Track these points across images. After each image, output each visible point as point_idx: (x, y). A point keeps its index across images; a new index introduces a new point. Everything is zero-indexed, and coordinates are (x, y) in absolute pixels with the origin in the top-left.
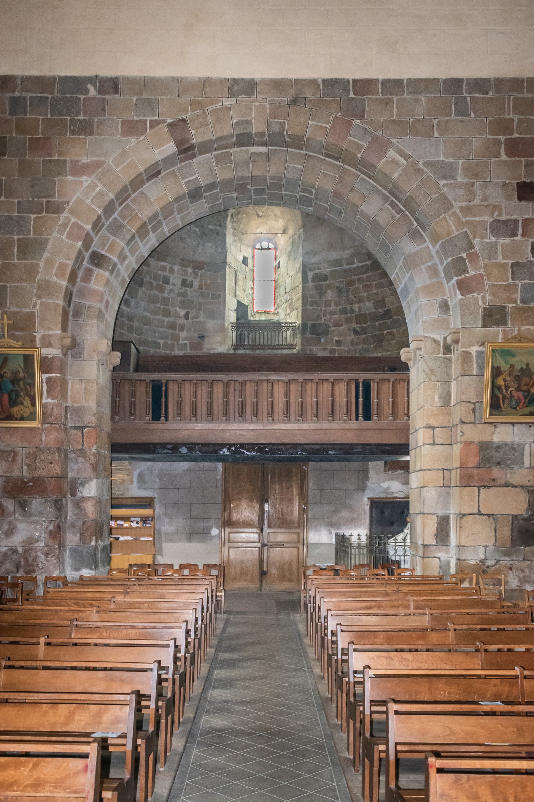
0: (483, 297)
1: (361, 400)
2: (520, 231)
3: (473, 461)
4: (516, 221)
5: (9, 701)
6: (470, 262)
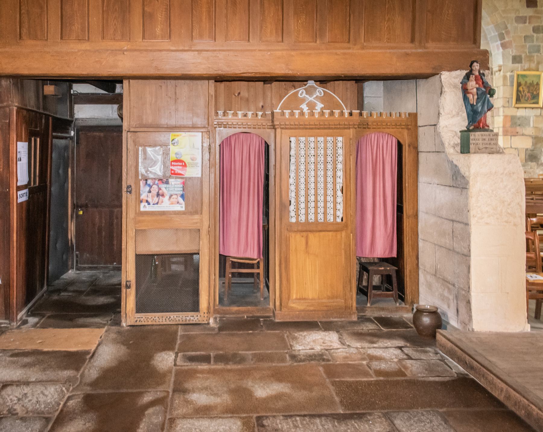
0: (512, 51)
1: (47, 222)
2: (528, 21)
3: (508, 124)
4: (526, 17)
5: (381, 246)
6: (506, 34)
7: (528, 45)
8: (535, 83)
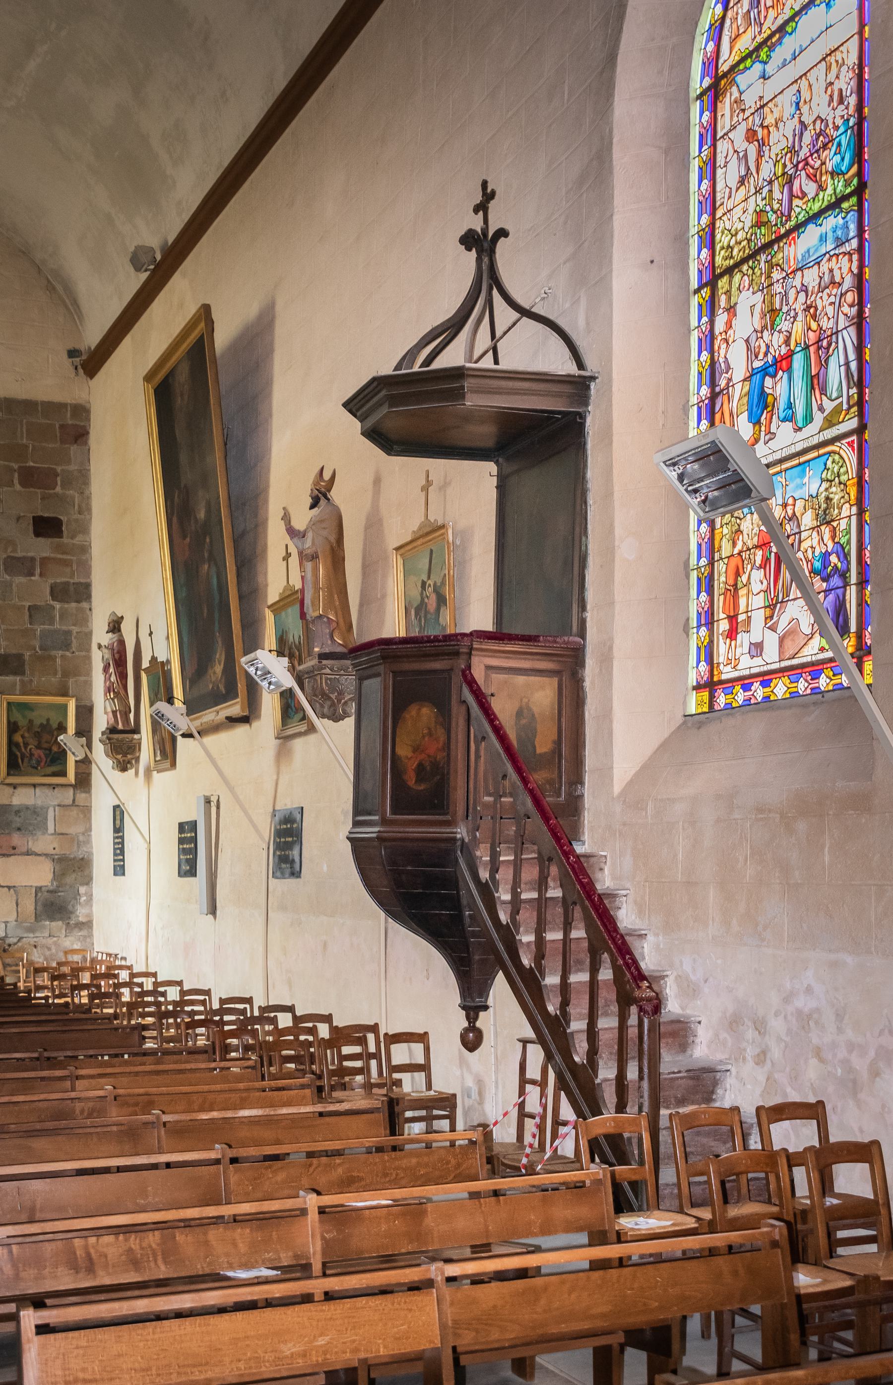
2: (38, 571)
4: (33, 559)
7: (39, 629)
8: (55, 726)
